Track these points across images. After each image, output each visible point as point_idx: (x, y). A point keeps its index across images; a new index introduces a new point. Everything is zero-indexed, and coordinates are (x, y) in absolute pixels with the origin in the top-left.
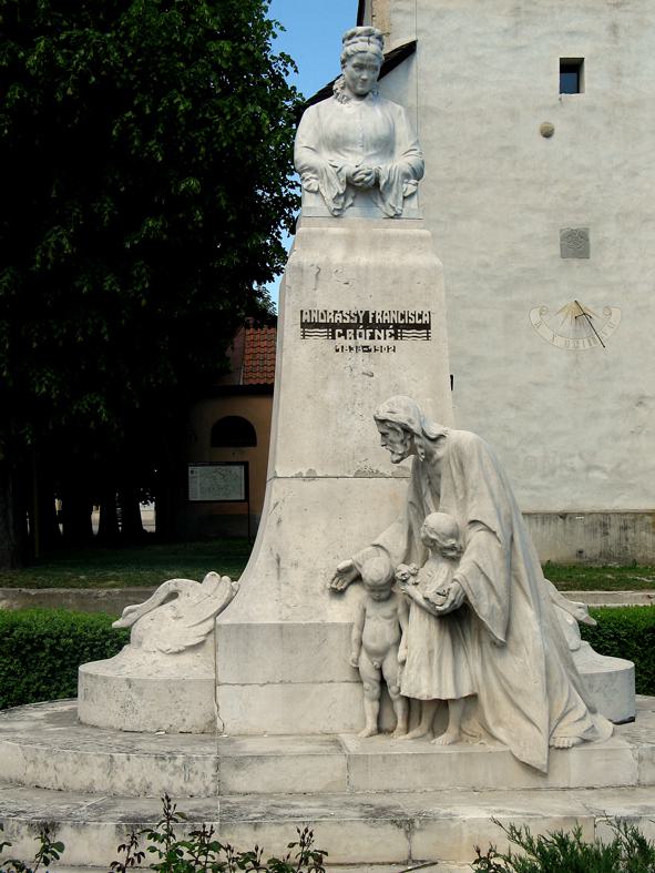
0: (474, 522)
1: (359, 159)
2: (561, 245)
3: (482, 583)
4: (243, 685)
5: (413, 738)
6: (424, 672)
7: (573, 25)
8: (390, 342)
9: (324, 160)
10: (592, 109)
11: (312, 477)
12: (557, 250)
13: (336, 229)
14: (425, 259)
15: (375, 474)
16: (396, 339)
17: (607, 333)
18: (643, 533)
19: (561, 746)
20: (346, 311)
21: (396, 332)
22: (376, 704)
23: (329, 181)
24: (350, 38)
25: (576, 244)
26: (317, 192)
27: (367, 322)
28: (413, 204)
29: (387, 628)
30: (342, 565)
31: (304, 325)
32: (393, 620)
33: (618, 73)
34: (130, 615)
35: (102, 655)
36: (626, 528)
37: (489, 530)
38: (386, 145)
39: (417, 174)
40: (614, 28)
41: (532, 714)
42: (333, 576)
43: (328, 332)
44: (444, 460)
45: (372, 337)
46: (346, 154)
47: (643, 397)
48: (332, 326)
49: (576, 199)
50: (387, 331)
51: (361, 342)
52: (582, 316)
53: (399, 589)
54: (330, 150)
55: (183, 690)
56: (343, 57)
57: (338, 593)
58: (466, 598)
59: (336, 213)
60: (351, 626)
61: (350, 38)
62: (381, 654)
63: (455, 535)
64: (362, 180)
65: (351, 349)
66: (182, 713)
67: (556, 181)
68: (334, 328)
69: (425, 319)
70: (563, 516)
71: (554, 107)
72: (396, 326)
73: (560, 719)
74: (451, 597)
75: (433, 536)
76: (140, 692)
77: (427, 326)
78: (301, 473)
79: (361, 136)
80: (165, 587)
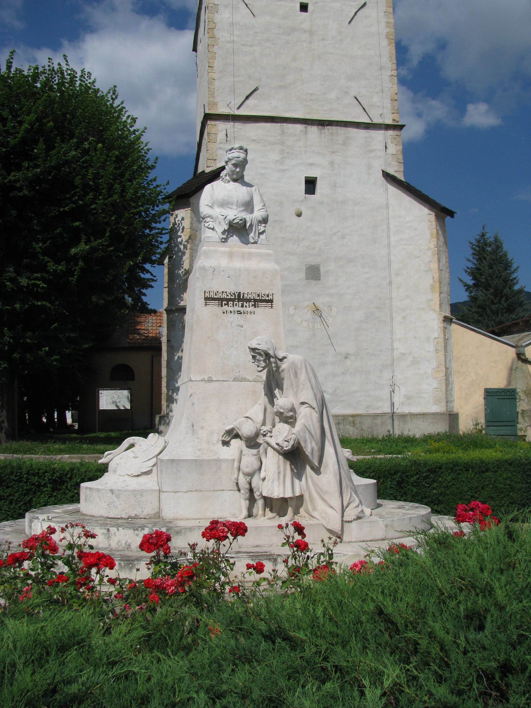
0: (303, 403)
1: (235, 212)
2: (306, 273)
3: (307, 435)
4: (176, 492)
5: (269, 519)
6: (276, 483)
7: (311, 161)
8: (252, 309)
9: (217, 211)
10: (321, 203)
11: (210, 380)
12: (303, 275)
13: (224, 248)
14: (270, 266)
15: (243, 380)
16: (255, 307)
17: (330, 320)
18: (348, 426)
19: (348, 520)
20: (233, 292)
21: (255, 304)
22: (247, 502)
23: (220, 223)
24: (230, 150)
26: (213, 229)
28: (263, 237)
29: (254, 460)
30: (228, 428)
31: (206, 299)
32: (257, 456)
33: (334, 186)
34: (108, 456)
35: (91, 479)
36: (339, 424)
37: (311, 407)
38: (249, 206)
39: (265, 221)
40: (332, 163)
41: (333, 504)
42: (223, 433)
43: (219, 303)
44: (286, 371)
45: (242, 306)
46: (228, 209)
47: (348, 354)
48: (221, 300)
49: (314, 249)
50: (250, 303)
51: (237, 308)
52: (317, 310)
53: (260, 440)
54: (219, 207)
55: (142, 495)
56: (227, 160)
57: (226, 443)
58: (299, 443)
59: (223, 240)
60: (234, 460)
61: (230, 150)
62: (251, 475)
63: (293, 410)
64: (238, 222)
65: (231, 312)
66: (141, 507)
67: (303, 239)
68: (222, 301)
69: (270, 297)
71: (302, 201)
72: (255, 301)
73: (347, 507)
74: (292, 442)
75: (282, 411)
76: (118, 497)
77: (271, 301)
78: (204, 379)
79: (236, 200)
80: (133, 439)
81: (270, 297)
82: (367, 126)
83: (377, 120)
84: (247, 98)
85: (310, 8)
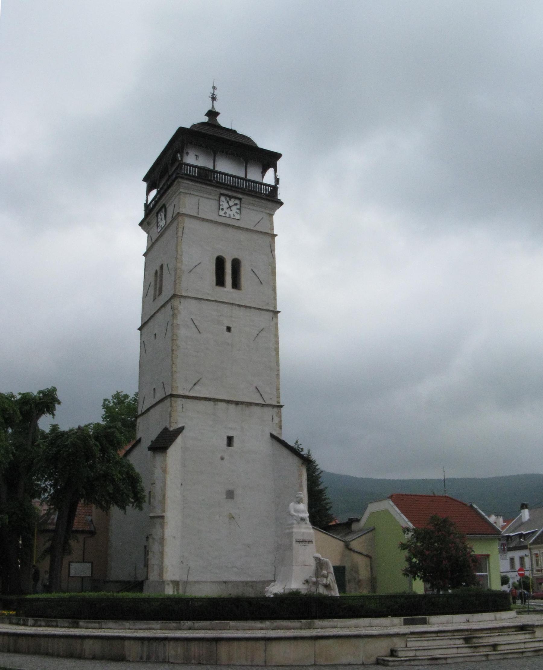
8: (307, 544)
12: (224, 496)
25: (230, 495)
27: (304, 541)
52: (232, 518)
70: (225, 582)
72: (308, 542)
74: (501, 554)
81: (312, 541)
82: (263, 405)
83: (268, 402)
84: (195, 385)
85: (232, 329)
